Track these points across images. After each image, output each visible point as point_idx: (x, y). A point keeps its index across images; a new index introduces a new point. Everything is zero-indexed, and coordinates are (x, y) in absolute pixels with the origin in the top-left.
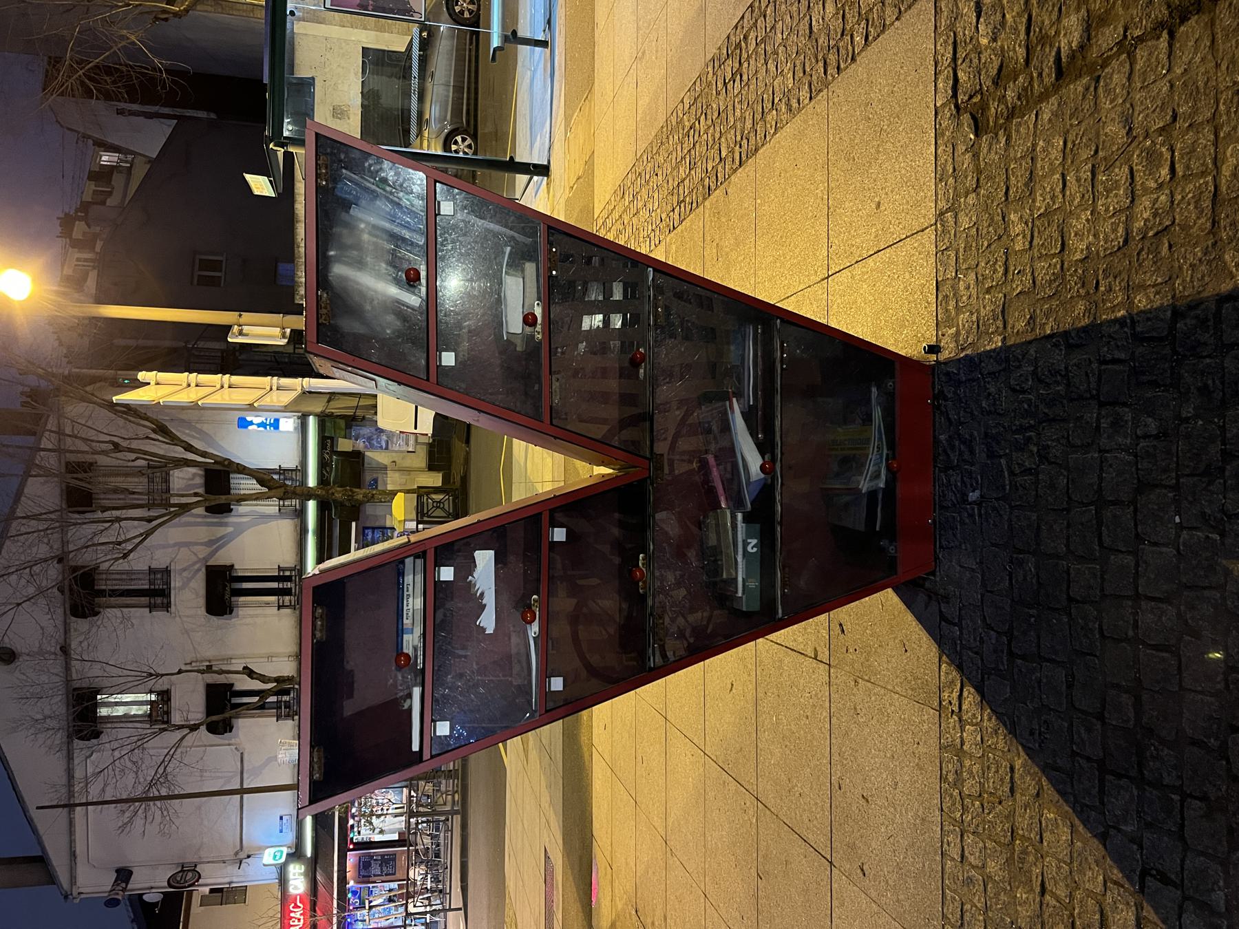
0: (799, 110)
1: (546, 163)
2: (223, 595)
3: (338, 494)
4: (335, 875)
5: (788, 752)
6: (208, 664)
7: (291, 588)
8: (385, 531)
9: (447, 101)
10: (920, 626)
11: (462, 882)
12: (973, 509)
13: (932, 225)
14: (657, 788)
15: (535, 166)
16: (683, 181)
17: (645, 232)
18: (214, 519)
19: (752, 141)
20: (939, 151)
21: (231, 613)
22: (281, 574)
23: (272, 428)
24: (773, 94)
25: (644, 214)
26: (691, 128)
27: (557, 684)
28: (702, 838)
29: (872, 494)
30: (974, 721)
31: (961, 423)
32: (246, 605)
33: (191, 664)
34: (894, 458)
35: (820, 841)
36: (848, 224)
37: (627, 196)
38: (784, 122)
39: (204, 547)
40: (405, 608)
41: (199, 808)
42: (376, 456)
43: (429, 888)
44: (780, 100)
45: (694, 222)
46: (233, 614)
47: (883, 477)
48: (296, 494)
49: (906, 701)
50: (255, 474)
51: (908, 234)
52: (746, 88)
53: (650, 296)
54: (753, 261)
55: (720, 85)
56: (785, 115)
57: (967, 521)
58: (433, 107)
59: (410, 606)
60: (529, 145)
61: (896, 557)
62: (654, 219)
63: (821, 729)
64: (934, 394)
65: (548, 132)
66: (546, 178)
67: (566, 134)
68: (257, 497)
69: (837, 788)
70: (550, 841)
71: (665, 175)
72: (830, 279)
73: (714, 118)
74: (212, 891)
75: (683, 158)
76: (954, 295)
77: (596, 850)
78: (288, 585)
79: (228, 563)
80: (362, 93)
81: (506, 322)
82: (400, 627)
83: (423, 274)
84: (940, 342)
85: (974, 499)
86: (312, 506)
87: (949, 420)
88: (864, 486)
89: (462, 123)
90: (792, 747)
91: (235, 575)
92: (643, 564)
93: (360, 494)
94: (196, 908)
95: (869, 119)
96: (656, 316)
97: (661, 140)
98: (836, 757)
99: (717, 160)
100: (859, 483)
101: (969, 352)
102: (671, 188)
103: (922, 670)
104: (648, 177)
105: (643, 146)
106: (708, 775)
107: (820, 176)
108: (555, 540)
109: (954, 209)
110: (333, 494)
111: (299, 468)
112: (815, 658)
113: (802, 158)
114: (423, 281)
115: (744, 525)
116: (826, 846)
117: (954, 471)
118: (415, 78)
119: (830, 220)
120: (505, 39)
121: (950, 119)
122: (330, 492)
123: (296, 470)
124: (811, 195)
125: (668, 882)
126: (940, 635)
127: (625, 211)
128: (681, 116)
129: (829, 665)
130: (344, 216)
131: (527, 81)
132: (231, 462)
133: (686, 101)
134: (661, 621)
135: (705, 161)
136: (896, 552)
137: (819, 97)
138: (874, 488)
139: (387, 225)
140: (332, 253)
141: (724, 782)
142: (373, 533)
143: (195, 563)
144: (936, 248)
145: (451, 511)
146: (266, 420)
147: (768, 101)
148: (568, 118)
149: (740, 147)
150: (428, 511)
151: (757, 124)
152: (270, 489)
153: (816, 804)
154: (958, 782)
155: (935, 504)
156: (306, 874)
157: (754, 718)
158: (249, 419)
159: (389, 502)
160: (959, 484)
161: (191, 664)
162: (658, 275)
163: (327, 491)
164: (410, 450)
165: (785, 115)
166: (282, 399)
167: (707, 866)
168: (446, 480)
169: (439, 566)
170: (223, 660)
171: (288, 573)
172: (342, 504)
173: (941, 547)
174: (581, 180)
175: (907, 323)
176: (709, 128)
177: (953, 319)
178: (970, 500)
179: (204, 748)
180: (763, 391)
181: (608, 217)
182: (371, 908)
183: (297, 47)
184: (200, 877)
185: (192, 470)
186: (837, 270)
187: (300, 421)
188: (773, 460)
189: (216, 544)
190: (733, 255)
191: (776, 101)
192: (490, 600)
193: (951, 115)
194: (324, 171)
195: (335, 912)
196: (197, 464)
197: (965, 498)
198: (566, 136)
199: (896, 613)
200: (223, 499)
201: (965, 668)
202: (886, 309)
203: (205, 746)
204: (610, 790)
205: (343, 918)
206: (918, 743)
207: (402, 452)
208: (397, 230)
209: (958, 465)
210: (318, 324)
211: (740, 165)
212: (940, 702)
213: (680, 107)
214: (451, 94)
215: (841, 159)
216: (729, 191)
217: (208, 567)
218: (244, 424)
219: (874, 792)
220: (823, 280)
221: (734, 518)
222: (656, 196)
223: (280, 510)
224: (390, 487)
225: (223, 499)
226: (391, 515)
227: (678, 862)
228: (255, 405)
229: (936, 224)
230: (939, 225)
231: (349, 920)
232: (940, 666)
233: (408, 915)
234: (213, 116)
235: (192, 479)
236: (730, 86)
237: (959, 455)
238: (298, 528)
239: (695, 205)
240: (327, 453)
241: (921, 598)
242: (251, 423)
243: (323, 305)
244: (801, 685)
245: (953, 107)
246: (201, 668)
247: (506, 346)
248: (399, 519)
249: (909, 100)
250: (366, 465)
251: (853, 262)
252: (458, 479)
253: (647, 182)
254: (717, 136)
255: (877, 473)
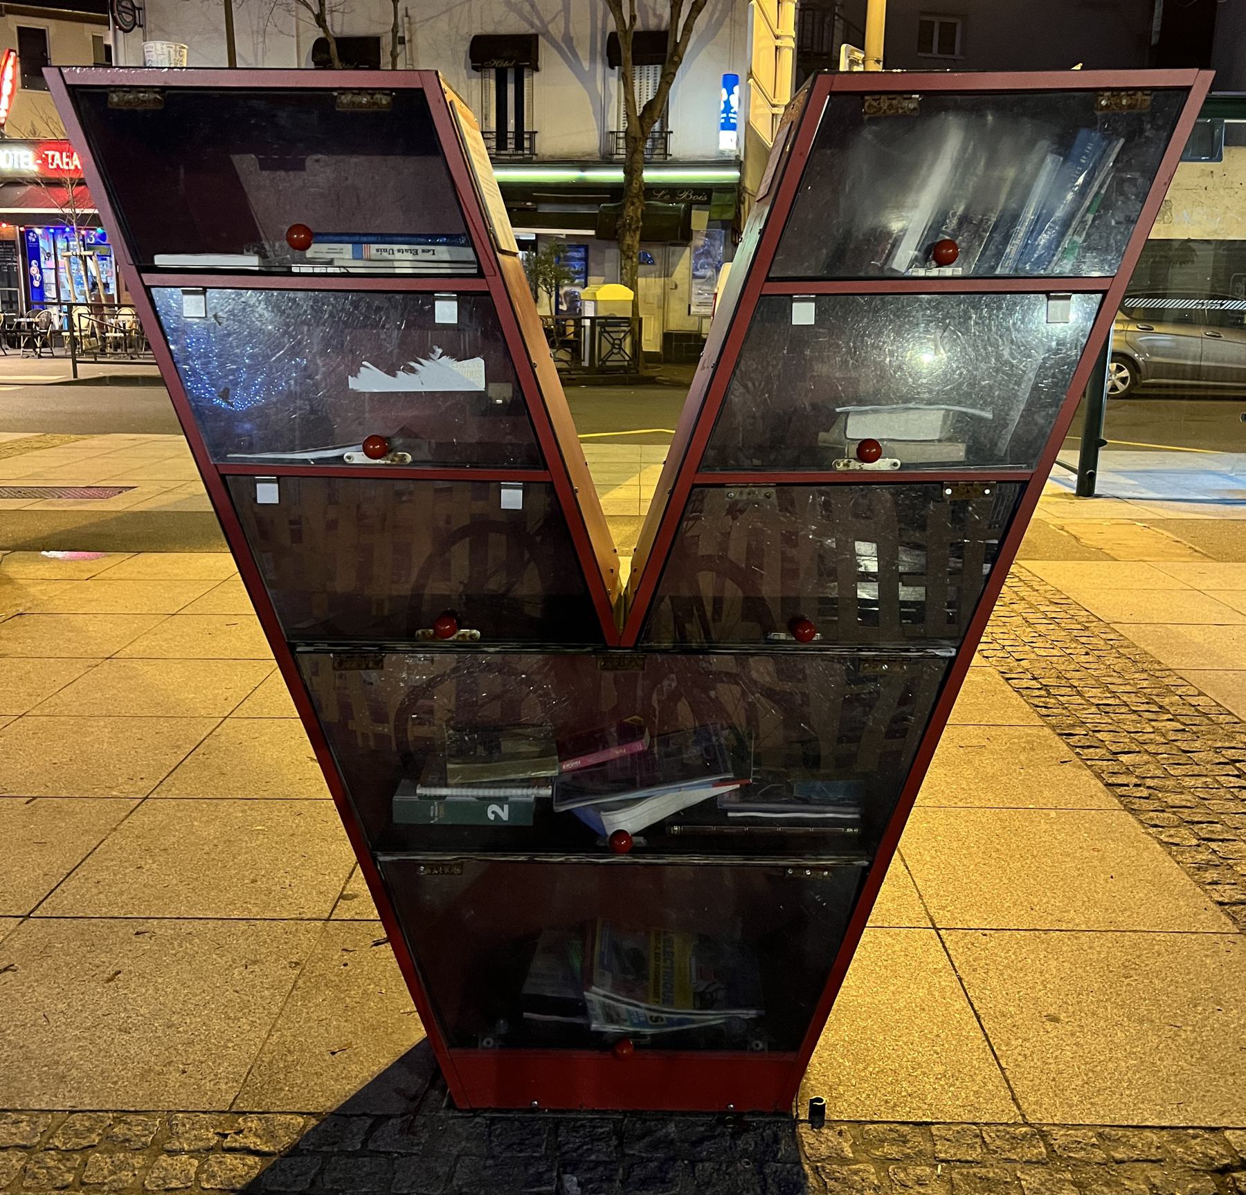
0: (1200, 884)
1: (1096, 492)
2: (498, 58)
3: (633, 211)
5: (206, 849)
6: (406, 39)
7: (506, 149)
8: (583, 275)
9: (1179, 357)
10: (370, 1079)
11: (111, 378)
12: (550, 1184)
13: (1023, 1116)
14: (187, 645)
15: (1093, 476)
16: (1079, 694)
17: (1001, 636)
18: (600, 45)
19: (1145, 805)
20: (1147, 1133)
21: (475, 68)
22: (526, 136)
23: (723, 121)
24: (1222, 841)
25: (1027, 634)
26: (1161, 707)
27: (268, 493)
28: (104, 712)
29: (581, 1008)
30: (204, 1176)
31: (693, 1164)
32: (484, 88)
33: (407, 16)
34: (637, 1047)
35: (65, 901)
36: (1020, 965)
37: (1052, 608)
38: (1180, 858)
39: (563, 31)
40: (396, 247)
41: (216, 30)
42: (684, 262)
43: (107, 335)
44: (1214, 851)
45: (1017, 710)
46: (474, 72)
47: (611, 1028)
48: (633, 154)
49: (254, 1050)
50: (661, 97)
51: (1007, 1073)
52: (1229, 796)
53: (907, 650)
54: (960, 804)
55: (1230, 753)
56: (1190, 860)
57: (531, 1171)
58: (1169, 338)
59: (398, 256)
60: (1121, 468)
61: (476, 1046)
62: (1020, 649)
63: (233, 903)
64: (743, 1114)
65: (1141, 496)
66: (1075, 492)
67: (1141, 521)
68: (629, 102)
69: (141, 929)
70: (142, 494)
71: (1087, 666)
72: (933, 931)
73: (1178, 744)
74: (108, 48)
75: (1114, 695)
76: (907, 1156)
77: (119, 557)
78: (511, 145)
79: (541, 63)
80: (1189, 240)
81: (866, 412)
82: (365, 239)
83: (948, 271)
84: (829, 1128)
85: (567, 1185)
86: (617, 176)
87: (701, 1141)
88: (596, 995)
89: (1148, 378)
90: (213, 856)
91: (526, 74)
92: (464, 635)
93: (633, 240)
94: (90, 30)
95: (1195, 1006)
96: (876, 661)
97: (1140, 661)
98: (186, 927)
99: (1114, 748)
100: (602, 986)
101: (812, 1181)
102: (1068, 676)
103: (299, 1082)
104: (1083, 640)
105: (1129, 632)
106: (194, 722)
107: (1096, 917)
108: (503, 491)
109: (1052, 1159)
110: (633, 204)
111: (669, 158)
112: (342, 897)
113: (1124, 887)
114: (935, 272)
115: (532, 799)
116: (54, 909)
117: (616, 1147)
118: (1222, 305)
119: (1027, 933)
121: (1205, 1155)
122: (636, 200)
123: (666, 154)
124: (1066, 901)
125: (52, 660)
126: (352, 1116)
127: (1031, 606)
128: (1179, 692)
129: (328, 920)
130: (1044, 144)
131: (1214, 466)
132: (677, 65)
133: (1200, 701)
134: (371, 665)
135: (1112, 728)
136: (484, 1048)
137: (1224, 918)
138: (591, 1012)
139: (1029, 215)
140: (990, 118)
141: (178, 747)
142: (580, 259)
143: (542, 21)
144: (986, 1124)
145: (608, 364)
146: (735, 113)
147: (1212, 832)
148: (1164, 523)
149: (1136, 785)
150: (608, 333)
151: (1174, 813)
152: (641, 117)
153: (122, 893)
154: (111, 1143)
155: (562, 1112)
157: (265, 795)
158: (736, 89)
159: (622, 279)
160: (593, 1157)
161: (407, 16)
162: (944, 665)
163: (637, 196)
164: (693, 309)
165: (1190, 860)
166: (760, 120)
167: (62, 719)
168: (651, 357)
169: (457, 299)
170: (412, 59)
171: (526, 144)
172: (619, 216)
173: (493, 1120)
174: (1074, 542)
175: (861, 1066)
176: (1164, 735)
177: (866, 1152)
178: (566, 1177)
179: (295, 34)
180: (750, 835)
181: (1021, 580)
182: (84, 259)
184: (126, 31)
185: (667, 13)
186: (947, 946)
187: (733, 159)
188: (635, 851)
189: (567, 48)
190: (968, 772)
191: (1214, 845)
192: (403, 383)
193: (1212, 1159)
194: (1124, 102)
195: (78, 211)
196: (675, 18)
197: (569, 1169)
198: (1137, 520)
199: (395, 1037)
200: (627, 54)
201: (292, 1160)
202: (886, 1029)
203: (298, 36)
204: (197, 577)
205: (70, 222)
206: (184, 1072)
207: (690, 297)
208: (1022, 230)
209: (624, 1155)
210: (862, 94)
211: (1107, 785)
212: (244, 1113)
213: (1192, 691)
214: (1189, 362)
215: (1126, 953)
216: (1067, 766)
217: (535, 37)
218: (730, 82)
219: (122, 991)
220: (931, 920)
221: (546, 782)
222: (1055, 652)
223: (612, 133)
224: (641, 281)
225: (627, 54)
226: (605, 283)
227: (77, 675)
228: (751, 81)
229: (1026, 1124)
230: (1024, 1129)
231: (67, 230)
232: (302, 1114)
233: (70, 306)
234: (1155, 40)
235: (655, 14)
236: (1230, 769)
237: (642, 1158)
238: (586, 158)
239: (1044, 711)
240: (689, 196)
241: (414, 1083)
242: (730, 92)
243: (894, 102)
244: (304, 872)
245: (1226, 1161)
246: (400, 29)
247: (828, 418)
248: (597, 293)
249: (1231, 1080)
250: (672, 248)
251: (960, 972)
252: (651, 373)
253: (1075, 639)
254: (1152, 748)
255: (615, 1017)
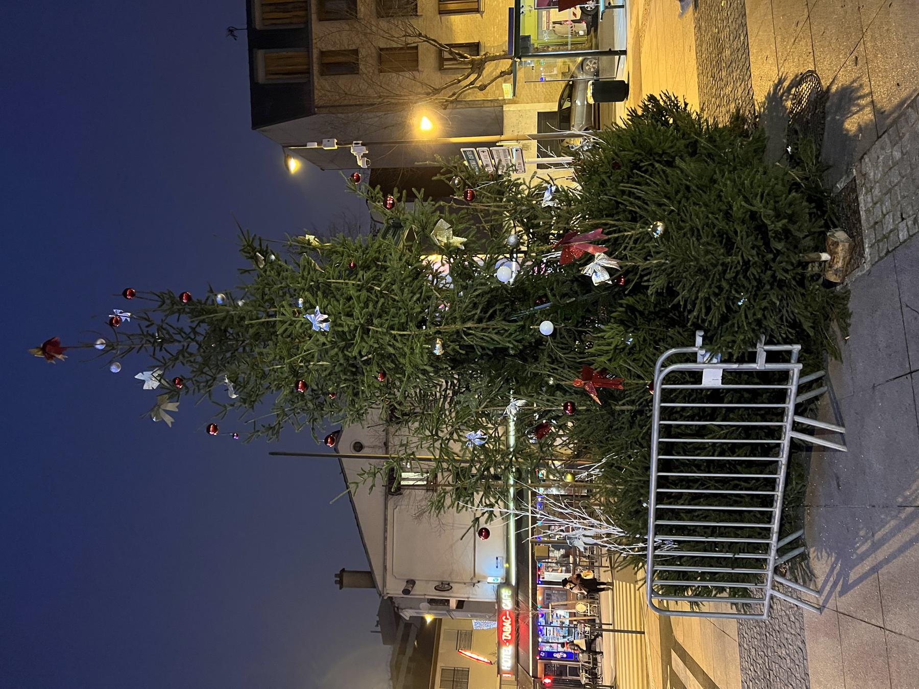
4: (530, 591)
120: (606, 8)
156: (512, 596)
183: (505, 117)
